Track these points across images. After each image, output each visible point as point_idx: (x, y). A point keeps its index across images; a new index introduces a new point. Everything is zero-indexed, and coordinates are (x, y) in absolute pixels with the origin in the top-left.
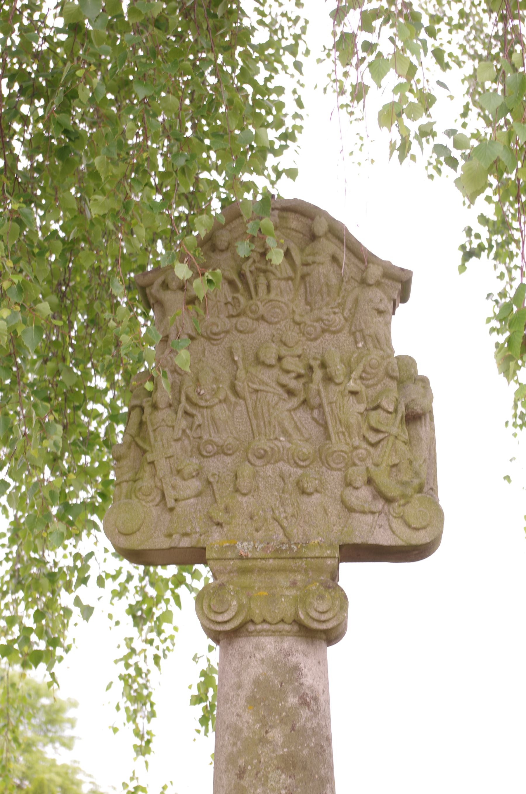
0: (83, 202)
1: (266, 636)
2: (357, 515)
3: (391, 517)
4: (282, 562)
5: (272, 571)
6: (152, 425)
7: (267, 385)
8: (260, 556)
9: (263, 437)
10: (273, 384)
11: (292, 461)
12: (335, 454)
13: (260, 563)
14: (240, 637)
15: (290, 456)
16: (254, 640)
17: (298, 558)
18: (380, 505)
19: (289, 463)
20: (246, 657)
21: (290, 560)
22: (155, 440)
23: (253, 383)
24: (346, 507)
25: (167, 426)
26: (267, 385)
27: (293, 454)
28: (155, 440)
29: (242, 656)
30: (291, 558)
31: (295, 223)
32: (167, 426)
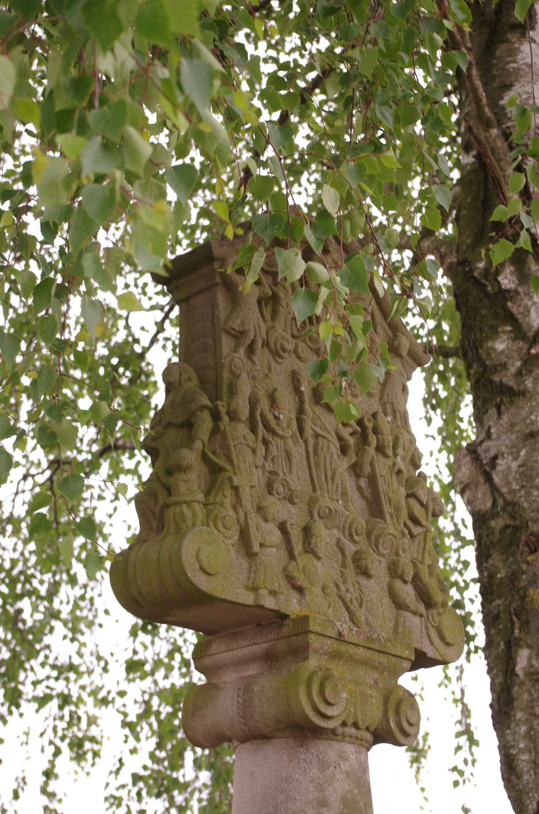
0: (59, 106)
1: (349, 743)
2: (409, 614)
3: (429, 625)
4: (369, 653)
5: (357, 662)
6: (233, 439)
7: (328, 433)
8: (354, 641)
9: (326, 494)
10: (333, 434)
11: (347, 532)
12: (388, 537)
13: (352, 650)
14: (319, 739)
15: (347, 526)
16: (337, 745)
17: (382, 652)
18: (422, 608)
19: (343, 533)
20: (329, 767)
21: (376, 653)
22: (238, 460)
23: (315, 425)
24: (394, 602)
25: (248, 446)
26: (328, 433)
27: (351, 523)
28: (238, 460)
29: (324, 765)
30: (379, 651)
31: (336, 255)
32: (248, 446)
